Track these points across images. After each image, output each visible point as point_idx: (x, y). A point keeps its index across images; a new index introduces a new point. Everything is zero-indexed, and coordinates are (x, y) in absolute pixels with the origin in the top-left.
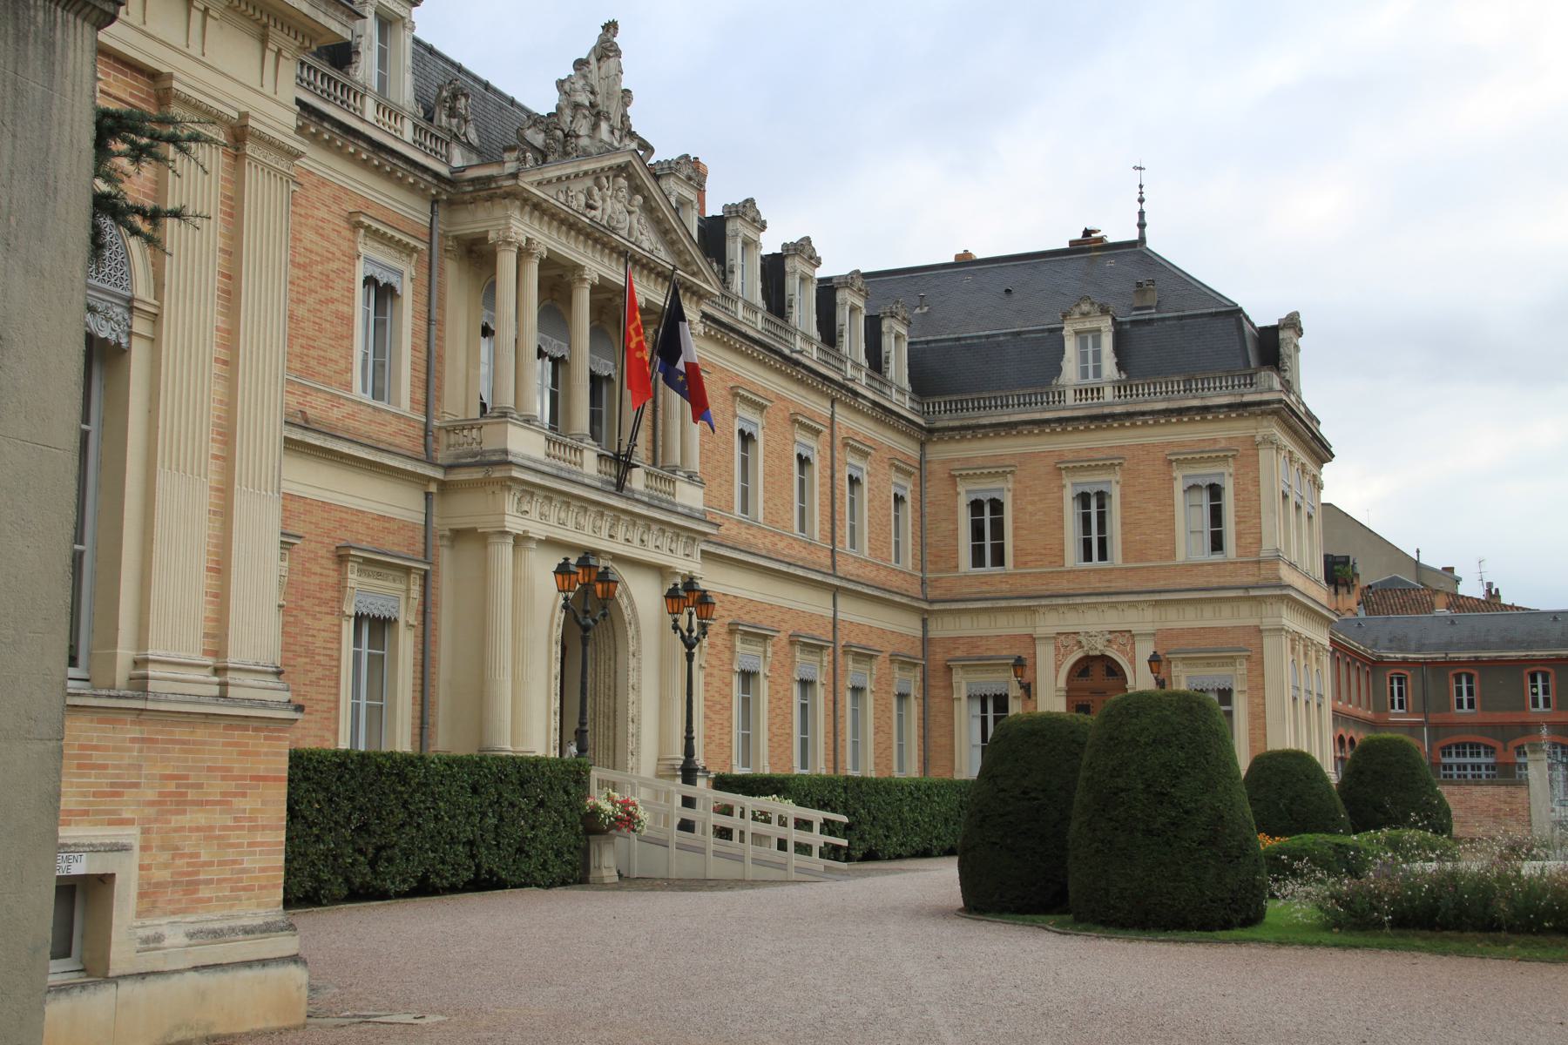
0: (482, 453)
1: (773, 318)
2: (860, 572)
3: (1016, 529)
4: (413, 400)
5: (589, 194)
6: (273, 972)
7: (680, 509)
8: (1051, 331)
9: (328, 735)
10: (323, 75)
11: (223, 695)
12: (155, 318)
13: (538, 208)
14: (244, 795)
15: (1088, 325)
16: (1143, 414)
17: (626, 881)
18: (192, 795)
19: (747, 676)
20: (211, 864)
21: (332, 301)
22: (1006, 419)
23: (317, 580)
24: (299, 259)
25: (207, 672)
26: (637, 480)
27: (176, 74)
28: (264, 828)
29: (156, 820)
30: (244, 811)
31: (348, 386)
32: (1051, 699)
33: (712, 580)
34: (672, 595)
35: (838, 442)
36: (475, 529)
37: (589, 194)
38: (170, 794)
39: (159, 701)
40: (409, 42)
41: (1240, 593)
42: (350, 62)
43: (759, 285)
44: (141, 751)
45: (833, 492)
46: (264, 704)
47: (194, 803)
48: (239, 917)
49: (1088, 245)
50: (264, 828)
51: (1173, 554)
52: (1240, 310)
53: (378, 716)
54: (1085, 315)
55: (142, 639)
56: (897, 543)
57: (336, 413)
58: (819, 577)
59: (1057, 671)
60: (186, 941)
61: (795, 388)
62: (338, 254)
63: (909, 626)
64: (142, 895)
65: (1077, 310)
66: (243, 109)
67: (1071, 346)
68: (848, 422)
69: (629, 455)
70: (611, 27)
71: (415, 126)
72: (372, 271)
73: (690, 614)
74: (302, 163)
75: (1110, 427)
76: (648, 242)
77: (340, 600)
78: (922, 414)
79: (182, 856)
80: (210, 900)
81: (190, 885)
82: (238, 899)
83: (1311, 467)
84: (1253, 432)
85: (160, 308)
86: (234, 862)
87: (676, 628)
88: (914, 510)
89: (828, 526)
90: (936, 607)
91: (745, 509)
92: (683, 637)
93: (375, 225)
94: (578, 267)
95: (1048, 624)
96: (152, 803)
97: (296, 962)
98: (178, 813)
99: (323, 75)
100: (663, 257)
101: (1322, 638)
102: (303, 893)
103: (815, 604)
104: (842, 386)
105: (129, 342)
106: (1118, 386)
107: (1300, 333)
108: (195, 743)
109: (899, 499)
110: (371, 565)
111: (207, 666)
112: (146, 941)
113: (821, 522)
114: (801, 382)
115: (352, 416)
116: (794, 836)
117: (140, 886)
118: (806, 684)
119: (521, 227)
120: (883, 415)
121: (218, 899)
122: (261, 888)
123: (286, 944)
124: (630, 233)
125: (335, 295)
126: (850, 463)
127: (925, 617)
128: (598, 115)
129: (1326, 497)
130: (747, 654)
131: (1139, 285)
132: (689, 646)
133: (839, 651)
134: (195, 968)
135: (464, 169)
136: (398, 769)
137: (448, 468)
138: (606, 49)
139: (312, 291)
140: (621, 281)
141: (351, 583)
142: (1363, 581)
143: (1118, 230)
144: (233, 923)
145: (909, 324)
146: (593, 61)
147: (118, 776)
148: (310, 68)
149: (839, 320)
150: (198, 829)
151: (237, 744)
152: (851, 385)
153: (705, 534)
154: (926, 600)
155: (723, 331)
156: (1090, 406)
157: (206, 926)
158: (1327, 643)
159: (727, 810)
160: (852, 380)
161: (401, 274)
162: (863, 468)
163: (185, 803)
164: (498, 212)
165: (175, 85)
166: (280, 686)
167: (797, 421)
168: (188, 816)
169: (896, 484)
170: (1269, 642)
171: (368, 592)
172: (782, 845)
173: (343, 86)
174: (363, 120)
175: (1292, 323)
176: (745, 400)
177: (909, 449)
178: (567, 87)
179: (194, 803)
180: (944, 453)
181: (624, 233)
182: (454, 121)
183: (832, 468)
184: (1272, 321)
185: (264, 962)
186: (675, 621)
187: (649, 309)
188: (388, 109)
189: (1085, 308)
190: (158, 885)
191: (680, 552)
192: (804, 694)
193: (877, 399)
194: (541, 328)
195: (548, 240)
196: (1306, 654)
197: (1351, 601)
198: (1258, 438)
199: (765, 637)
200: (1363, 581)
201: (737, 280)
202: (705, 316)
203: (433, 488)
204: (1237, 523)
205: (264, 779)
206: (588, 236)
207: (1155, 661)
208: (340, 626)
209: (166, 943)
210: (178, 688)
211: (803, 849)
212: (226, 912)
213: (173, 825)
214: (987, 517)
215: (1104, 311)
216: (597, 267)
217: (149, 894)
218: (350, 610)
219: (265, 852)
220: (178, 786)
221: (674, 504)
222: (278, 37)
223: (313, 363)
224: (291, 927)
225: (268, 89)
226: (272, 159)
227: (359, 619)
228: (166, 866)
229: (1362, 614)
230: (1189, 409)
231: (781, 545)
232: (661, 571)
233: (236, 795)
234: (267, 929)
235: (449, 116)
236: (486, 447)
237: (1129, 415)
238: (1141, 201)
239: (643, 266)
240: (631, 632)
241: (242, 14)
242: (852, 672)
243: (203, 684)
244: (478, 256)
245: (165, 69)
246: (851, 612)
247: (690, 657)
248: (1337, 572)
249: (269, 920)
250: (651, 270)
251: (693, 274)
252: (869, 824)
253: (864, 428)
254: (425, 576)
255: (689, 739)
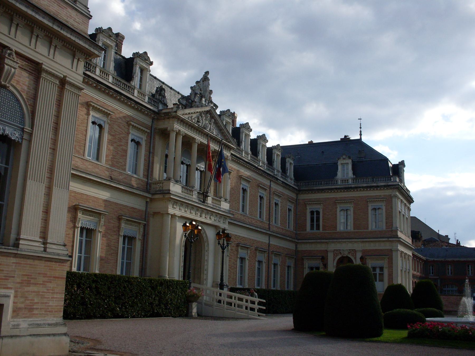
0: (163, 190)
1: (253, 156)
2: (277, 230)
3: (323, 219)
4: (143, 175)
5: (198, 118)
6: (57, 338)
7: (222, 210)
8: (335, 163)
9: (114, 270)
10: (123, 83)
11: (45, 251)
12: (31, 135)
13: (183, 122)
14: (51, 282)
15: (345, 161)
16: (360, 187)
17: (200, 315)
18: (32, 281)
19: (242, 259)
20: (38, 303)
21: (121, 145)
22: (321, 188)
23: (112, 225)
24: (112, 133)
25: (40, 243)
26: (209, 200)
27: (44, 63)
28: (57, 293)
29: (20, 288)
30: (50, 287)
31: (125, 170)
32: (332, 268)
33: (231, 230)
34: (218, 234)
35: (272, 193)
36: (160, 212)
37: (198, 118)
38: (26, 280)
39: (22, 251)
40: (148, 75)
41: (386, 239)
42: (131, 80)
43: (266, 157)
44: (16, 266)
45: (270, 207)
46: (58, 255)
47: (33, 284)
48: (47, 320)
49: (346, 140)
50: (57, 293)
51: (368, 228)
52: (388, 159)
53: (129, 266)
54: (344, 159)
55: (19, 233)
56: (289, 223)
57: (121, 177)
58: (265, 231)
59: (334, 261)
60: (28, 326)
61: (259, 177)
62: (124, 132)
63: (291, 246)
64: (14, 311)
65: (342, 158)
66: (65, 75)
67: (340, 167)
68: (274, 186)
69: (207, 192)
70: (207, 73)
71: (149, 98)
72: (133, 137)
73: (224, 240)
74: (84, 91)
75: (350, 191)
76: (215, 133)
77: (119, 231)
78: (297, 186)
79: (29, 300)
80: (37, 314)
81: (31, 309)
82: (48, 315)
83: (408, 204)
84: (391, 193)
85: (33, 131)
86: (46, 303)
87: (219, 244)
88: (294, 213)
89: (268, 217)
90: (300, 241)
91: (243, 211)
92: (221, 246)
93: (135, 125)
94: (194, 139)
95: (332, 247)
96: (19, 283)
97: (65, 335)
98: (27, 286)
99: (123, 83)
100: (219, 137)
101: (410, 253)
102: (68, 315)
103: (263, 239)
104: (273, 177)
105: (22, 141)
106: (353, 179)
107: (404, 166)
108: (34, 265)
109: (290, 210)
110: (87, 212)
111: (40, 242)
112: (14, 325)
113: (266, 216)
114: (261, 175)
115: (125, 178)
116: (250, 305)
117: (13, 308)
118: (260, 262)
119: (177, 126)
120: (286, 185)
121: (40, 314)
122: (55, 312)
123: (63, 330)
124: (210, 130)
125: (122, 144)
126: (276, 199)
127: (296, 244)
128: (202, 97)
129: (412, 214)
130: (242, 253)
131: (360, 151)
132: (223, 249)
133: (270, 253)
134: (30, 335)
135: (162, 110)
136: (128, 281)
137: (153, 194)
138: (206, 78)
139: (115, 142)
140: (206, 143)
141: (122, 226)
142: (424, 238)
143: (354, 136)
144: (44, 322)
145: (294, 160)
146: (201, 82)
147: (7, 274)
148: (119, 81)
149: (287, 166)
150: (34, 292)
151: (48, 266)
152: (276, 176)
153: (230, 217)
154: (297, 239)
155: (237, 160)
156: (345, 185)
157: (35, 322)
158: (411, 255)
159: (231, 297)
160: (276, 175)
161: (142, 139)
162: (279, 200)
163: (30, 283)
164: (171, 121)
165: (43, 66)
166: (65, 249)
167: (259, 186)
168: (31, 288)
169: (289, 206)
170: (394, 253)
171: (126, 229)
172: (246, 308)
173: (129, 86)
174: (133, 96)
175: (402, 164)
176: (276, 195)
177: (293, 195)
178: (193, 88)
179: (33, 284)
180: (303, 197)
181: (208, 129)
182: (160, 97)
183: (270, 200)
184: (397, 163)
185: (54, 335)
186: (219, 242)
187: (215, 151)
188: (142, 94)
189: (344, 157)
190: (20, 309)
191: (222, 222)
192: (259, 265)
193: (284, 181)
194: (182, 155)
195: (184, 130)
196: (405, 257)
197: (420, 244)
198: (392, 195)
199: (248, 248)
200: (424, 238)
201: (243, 146)
202: (232, 154)
203: (148, 200)
204: (386, 219)
205: (58, 278)
206: (197, 130)
207: (362, 258)
208: (119, 238)
209: (21, 327)
210: (29, 247)
211: (252, 309)
212: (43, 318)
213: (26, 290)
214: (315, 216)
215: (349, 158)
216: (199, 139)
217: (16, 311)
218: (122, 234)
219: (57, 300)
220: (28, 278)
221: (220, 208)
222: (78, 54)
223: (115, 163)
224: (65, 324)
225: (74, 69)
226: (73, 90)
227: (125, 237)
228: (23, 303)
229: (423, 247)
230: (373, 186)
231: (253, 222)
232: (216, 227)
233: (48, 282)
234: (56, 325)
235: (159, 96)
236: (164, 189)
237: (356, 188)
238: (361, 128)
239: (214, 139)
240: (206, 244)
241: (68, 48)
242: (275, 260)
243: (38, 247)
244: (165, 134)
245: (41, 62)
246: (274, 242)
247: (223, 252)
248: (415, 235)
249: (58, 322)
250: (216, 141)
251: (229, 142)
252: (272, 303)
253: (280, 189)
254: (145, 225)
255: (222, 276)
